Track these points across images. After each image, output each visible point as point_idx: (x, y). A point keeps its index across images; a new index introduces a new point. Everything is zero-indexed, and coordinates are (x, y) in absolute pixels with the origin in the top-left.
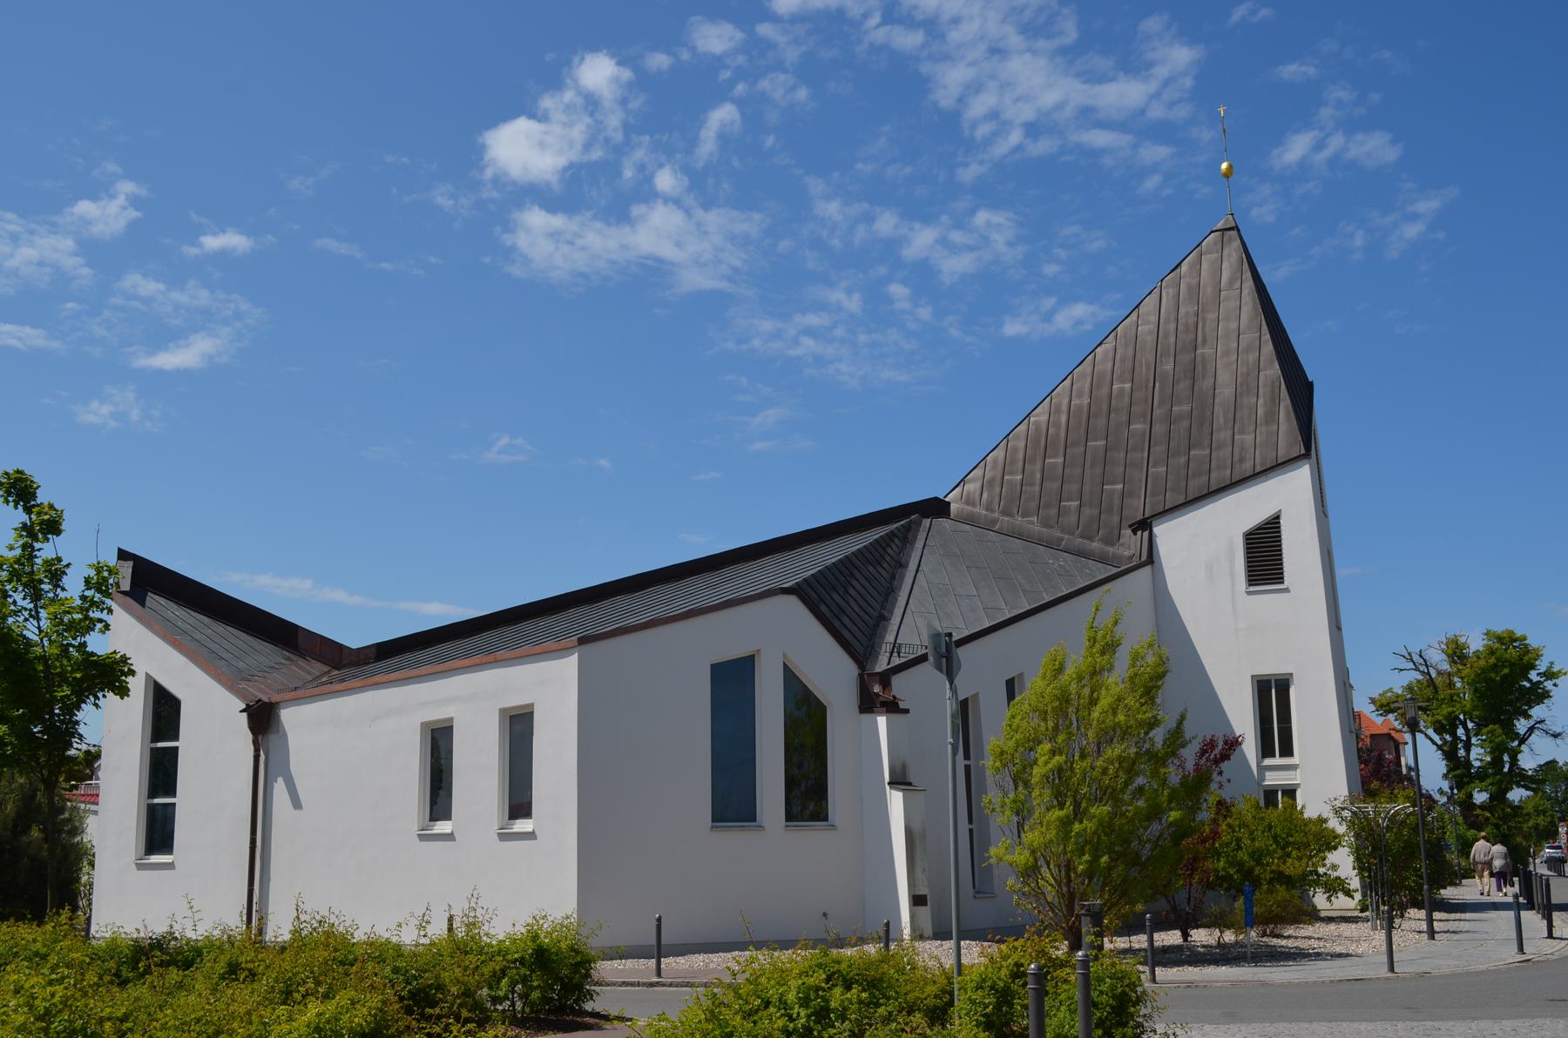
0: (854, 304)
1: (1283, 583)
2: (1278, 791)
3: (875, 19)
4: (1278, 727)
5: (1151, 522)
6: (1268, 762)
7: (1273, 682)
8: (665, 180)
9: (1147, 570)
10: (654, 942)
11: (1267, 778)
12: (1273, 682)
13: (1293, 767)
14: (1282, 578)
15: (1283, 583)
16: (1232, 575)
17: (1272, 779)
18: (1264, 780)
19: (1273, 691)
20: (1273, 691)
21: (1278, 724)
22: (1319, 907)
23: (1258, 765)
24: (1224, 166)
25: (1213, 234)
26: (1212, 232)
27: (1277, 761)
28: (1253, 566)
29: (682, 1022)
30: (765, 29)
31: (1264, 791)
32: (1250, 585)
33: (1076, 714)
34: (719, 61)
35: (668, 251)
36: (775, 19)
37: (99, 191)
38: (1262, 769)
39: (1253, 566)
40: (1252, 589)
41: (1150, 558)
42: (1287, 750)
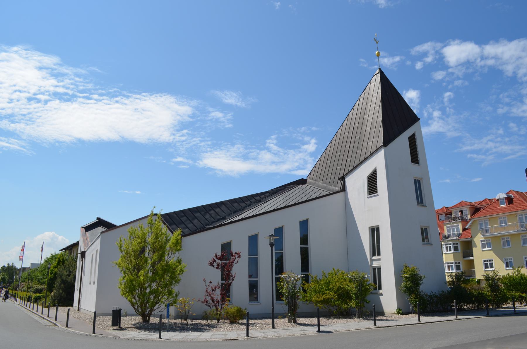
0: (501, 132)
1: (377, 193)
2: (376, 268)
3: (479, 60)
4: (377, 245)
5: (345, 177)
6: (374, 258)
7: (375, 229)
8: (436, 114)
9: (342, 194)
10: (271, 312)
11: (373, 264)
12: (375, 229)
13: (379, 260)
14: (377, 191)
15: (377, 193)
16: (364, 192)
17: (375, 264)
18: (372, 264)
19: (375, 232)
20: (375, 232)
21: (377, 244)
22: (385, 312)
23: (371, 259)
24: (377, 52)
25: (374, 77)
26: (374, 76)
27: (376, 257)
28: (370, 186)
29: (290, 332)
30: (450, 70)
31: (373, 268)
32: (369, 195)
33: (145, 257)
34: (442, 81)
35: (441, 130)
36: (451, 67)
37: (308, 143)
38: (372, 261)
39: (370, 186)
40: (370, 196)
41: (344, 189)
42: (379, 254)
